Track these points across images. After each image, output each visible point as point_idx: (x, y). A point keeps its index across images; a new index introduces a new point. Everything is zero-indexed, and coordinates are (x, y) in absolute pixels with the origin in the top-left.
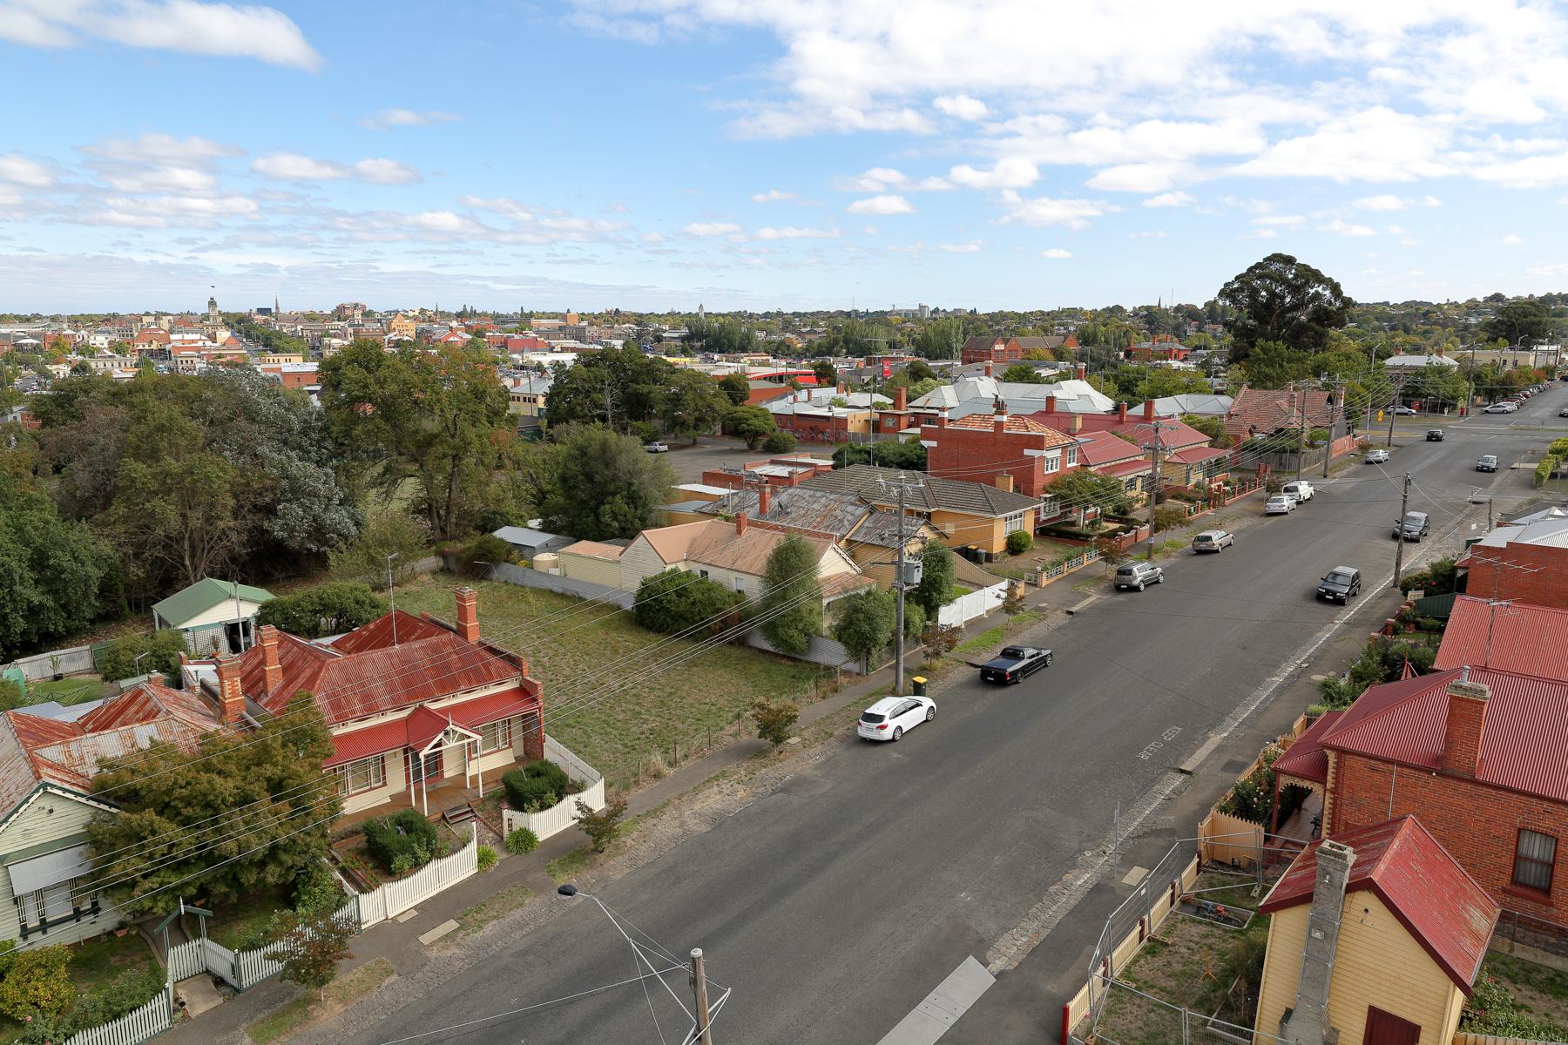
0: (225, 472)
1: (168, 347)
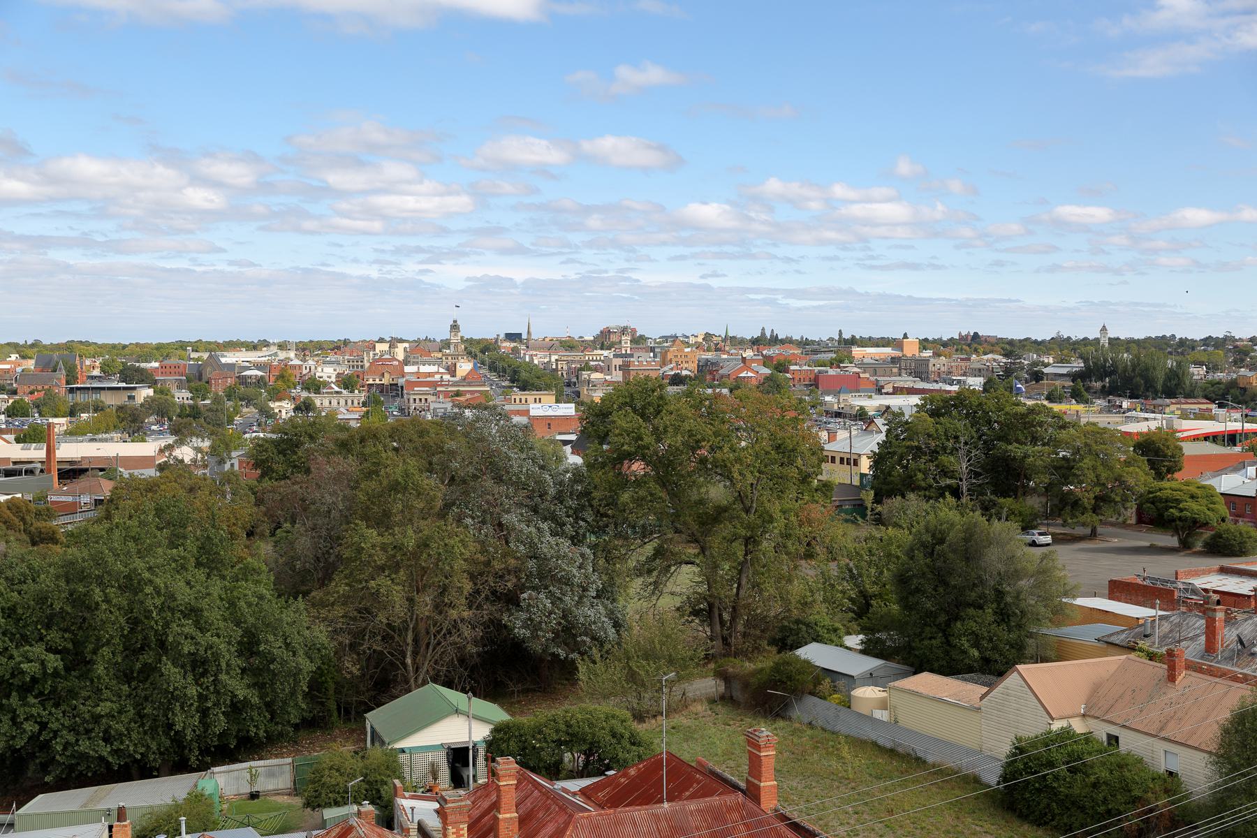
1: (401, 381)
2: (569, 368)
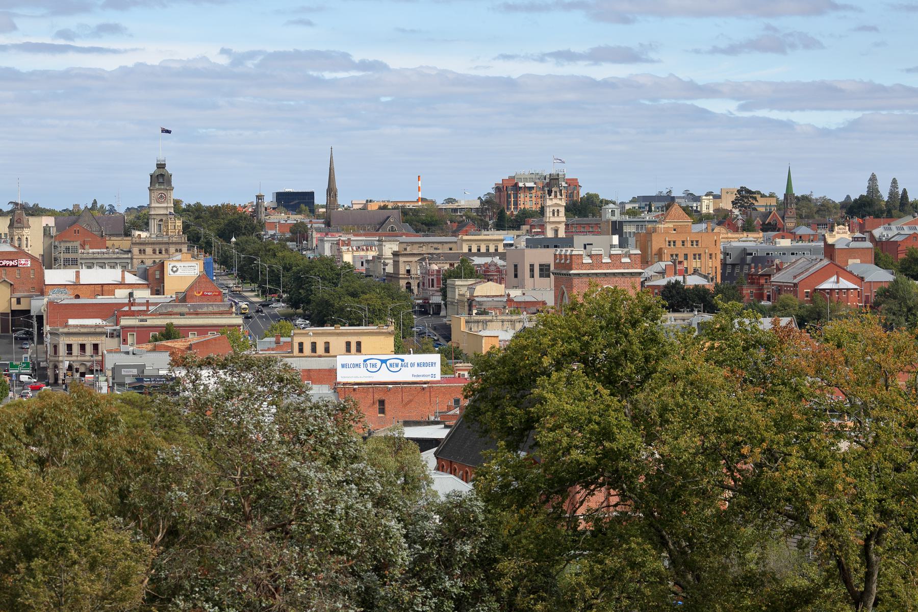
1: (38, 305)
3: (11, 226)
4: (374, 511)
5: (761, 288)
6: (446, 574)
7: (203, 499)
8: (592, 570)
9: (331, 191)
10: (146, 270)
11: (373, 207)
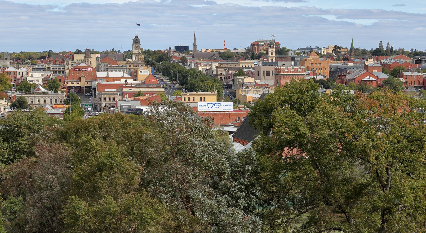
0: (159, 214)
1: (94, 84)
2: (227, 74)
3: (85, 57)
4: (218, 155)
5: (343, 80)
6: (243, 177)
7: (159, 151)
8: (292, 176)
9: (195, 46)
10: (131, 72)
11: (209, 51)
